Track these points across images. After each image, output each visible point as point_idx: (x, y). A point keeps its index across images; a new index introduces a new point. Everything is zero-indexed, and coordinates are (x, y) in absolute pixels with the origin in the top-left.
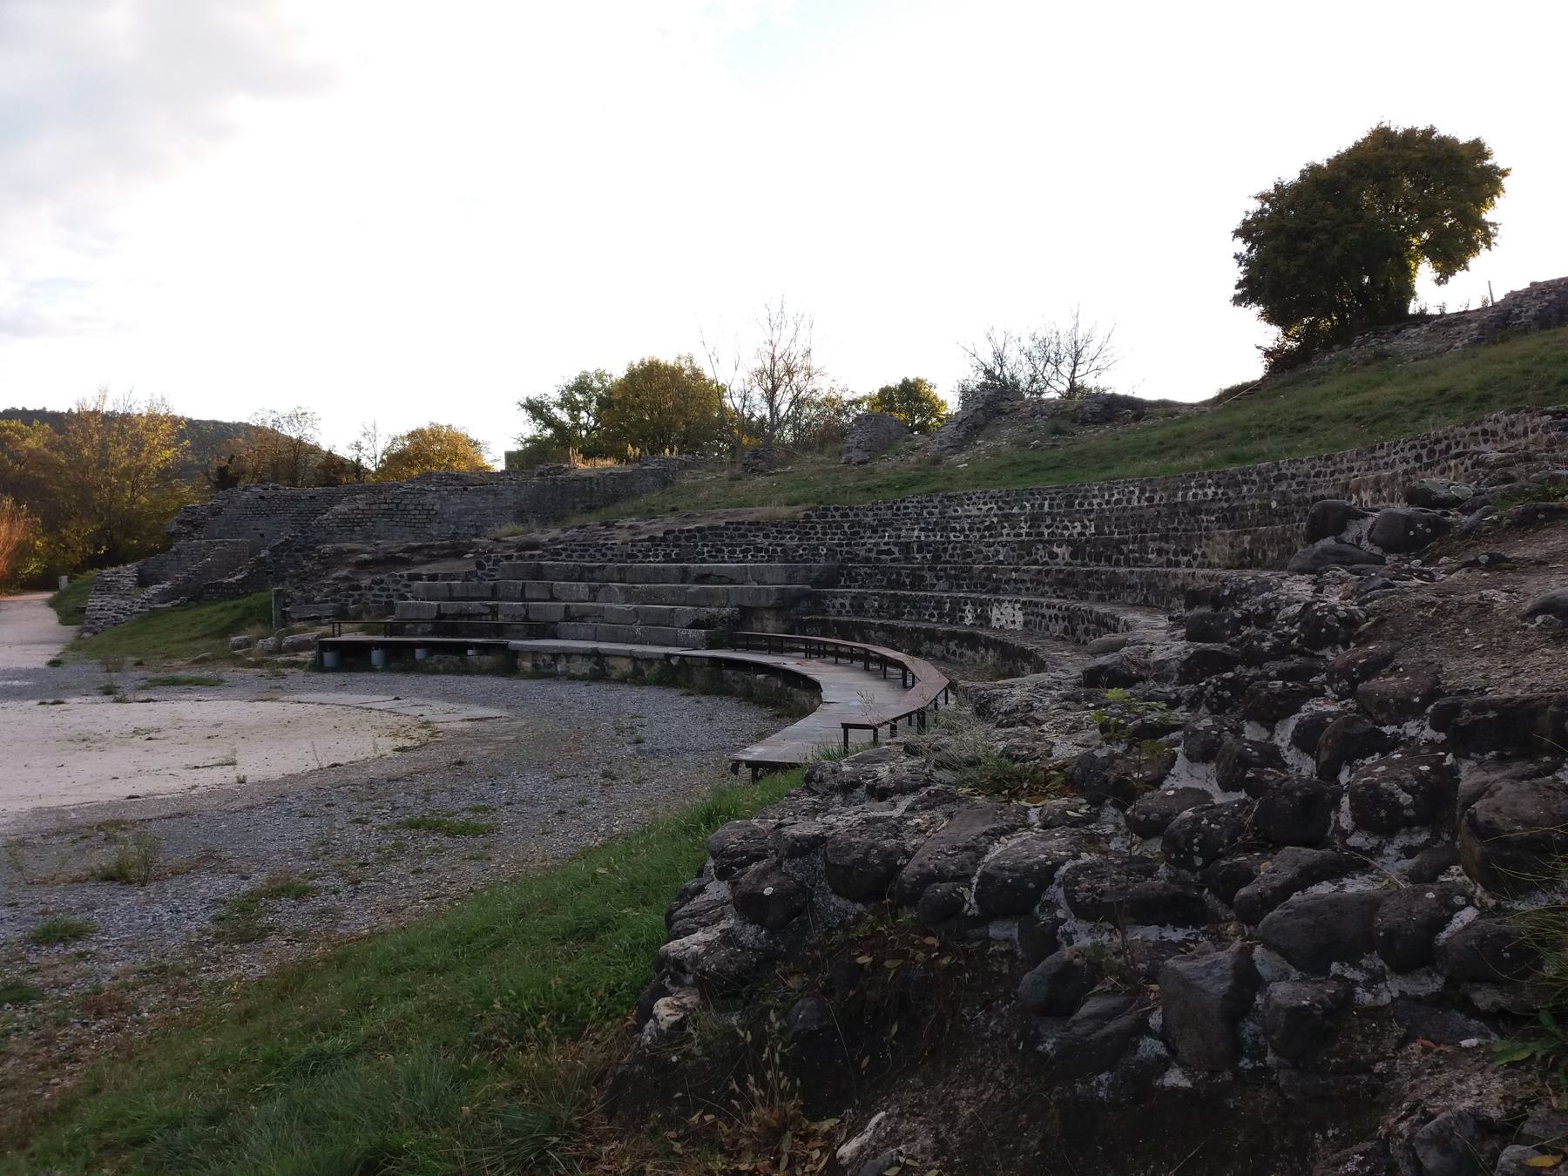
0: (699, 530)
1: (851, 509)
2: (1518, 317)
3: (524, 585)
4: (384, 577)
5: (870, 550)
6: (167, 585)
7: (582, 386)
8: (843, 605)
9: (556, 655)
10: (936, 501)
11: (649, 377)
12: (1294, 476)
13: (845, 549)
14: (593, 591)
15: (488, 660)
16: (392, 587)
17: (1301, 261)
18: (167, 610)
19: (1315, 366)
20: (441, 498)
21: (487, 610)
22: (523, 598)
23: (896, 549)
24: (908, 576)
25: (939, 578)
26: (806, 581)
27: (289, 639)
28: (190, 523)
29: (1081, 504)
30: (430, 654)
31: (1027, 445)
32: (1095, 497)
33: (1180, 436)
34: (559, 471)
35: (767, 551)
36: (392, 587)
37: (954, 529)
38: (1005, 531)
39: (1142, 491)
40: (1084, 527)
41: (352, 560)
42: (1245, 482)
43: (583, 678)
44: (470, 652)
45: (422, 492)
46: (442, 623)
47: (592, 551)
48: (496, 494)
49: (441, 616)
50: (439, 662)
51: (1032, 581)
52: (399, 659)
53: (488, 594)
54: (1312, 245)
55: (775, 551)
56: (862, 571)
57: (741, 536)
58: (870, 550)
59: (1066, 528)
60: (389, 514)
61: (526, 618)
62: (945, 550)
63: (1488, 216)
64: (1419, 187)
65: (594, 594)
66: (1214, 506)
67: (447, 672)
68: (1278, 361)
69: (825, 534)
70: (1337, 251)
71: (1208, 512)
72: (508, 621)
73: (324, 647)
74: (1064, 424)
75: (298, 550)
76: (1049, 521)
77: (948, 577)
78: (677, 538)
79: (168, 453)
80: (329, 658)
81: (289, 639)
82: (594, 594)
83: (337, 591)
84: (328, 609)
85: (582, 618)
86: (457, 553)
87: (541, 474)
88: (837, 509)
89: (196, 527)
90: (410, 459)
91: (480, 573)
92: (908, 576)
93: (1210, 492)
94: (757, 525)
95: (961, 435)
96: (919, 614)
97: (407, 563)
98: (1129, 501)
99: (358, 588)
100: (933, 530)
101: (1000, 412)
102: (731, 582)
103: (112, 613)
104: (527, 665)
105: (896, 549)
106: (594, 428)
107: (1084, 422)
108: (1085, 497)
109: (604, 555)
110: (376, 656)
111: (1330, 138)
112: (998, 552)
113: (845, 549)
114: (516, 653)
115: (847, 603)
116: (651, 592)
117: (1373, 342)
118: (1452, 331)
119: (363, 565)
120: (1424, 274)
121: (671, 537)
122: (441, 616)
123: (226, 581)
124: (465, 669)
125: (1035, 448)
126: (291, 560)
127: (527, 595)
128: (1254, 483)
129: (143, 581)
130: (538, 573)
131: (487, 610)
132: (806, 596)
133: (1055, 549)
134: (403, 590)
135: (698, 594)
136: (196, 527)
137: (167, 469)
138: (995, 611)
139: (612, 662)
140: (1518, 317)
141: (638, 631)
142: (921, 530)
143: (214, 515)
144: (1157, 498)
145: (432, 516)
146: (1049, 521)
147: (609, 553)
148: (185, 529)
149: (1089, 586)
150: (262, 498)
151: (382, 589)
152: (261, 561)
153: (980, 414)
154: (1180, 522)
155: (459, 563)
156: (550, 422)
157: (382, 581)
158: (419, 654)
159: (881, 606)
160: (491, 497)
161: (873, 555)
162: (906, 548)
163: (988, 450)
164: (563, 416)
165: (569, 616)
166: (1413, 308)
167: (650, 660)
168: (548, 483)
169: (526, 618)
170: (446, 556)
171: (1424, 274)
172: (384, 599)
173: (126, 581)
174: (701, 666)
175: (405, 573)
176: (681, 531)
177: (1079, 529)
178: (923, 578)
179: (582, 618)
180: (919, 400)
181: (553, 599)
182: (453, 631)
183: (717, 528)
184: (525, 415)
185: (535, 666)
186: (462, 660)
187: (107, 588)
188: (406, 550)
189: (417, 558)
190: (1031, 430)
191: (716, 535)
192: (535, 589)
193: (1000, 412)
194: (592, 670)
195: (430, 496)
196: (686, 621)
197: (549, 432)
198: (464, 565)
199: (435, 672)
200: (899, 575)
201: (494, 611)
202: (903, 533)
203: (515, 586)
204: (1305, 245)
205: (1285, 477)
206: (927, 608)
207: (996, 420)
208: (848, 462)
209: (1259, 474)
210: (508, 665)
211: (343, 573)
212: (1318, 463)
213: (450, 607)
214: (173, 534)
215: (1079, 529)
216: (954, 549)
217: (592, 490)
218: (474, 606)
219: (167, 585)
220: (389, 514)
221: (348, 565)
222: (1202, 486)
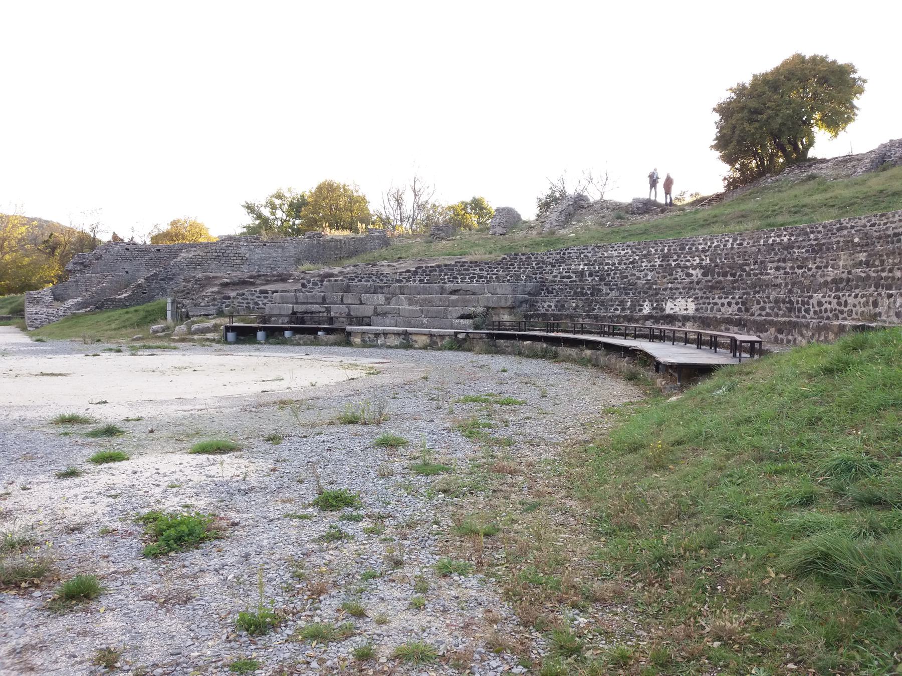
0: (438, 266)
1: (533, 255)
2: (890, 157)
3: (343, 296)
4: (244, 291)
5: (556, 276)
6: (79, 299)
7: (279, 196)
8: (550, 306)
9: (377, 335)
10: (590, 249)
11: (327, 190)
12: (852, 227)
13: (538, 276)
14: (387, 299)
15: (332, 338)
16: (250, 297)
17: (757, 125)
18: (83, 314)
19: (762, 183)
20: (250, 250)
21: (324, 310)
22: (342, 303)
23: (573, 275)
24: (589, 289)
25: (611, 290)
26: (523, 292)
27: (195, 326)
28: (82, 263)
29: (690, 248)
30: (294, 334)
31: (604, 224)
32: (700, 244)
33: (715, 216)
34: (320, 235)
35: (486, 278)
36: (250, 297)
37: (607, 264)
38: (644, 264)
39: (735, 240)
40: (702, 260)
41: (218, 282)
42: (812, 232)
43: (396, 347)
44: (320, 333)
45: (238, 246)
46: (295, 316)
47: (374, 278)
48: (283, 248)
49: (294, 313)
50: (300, 339)
51: (684, 288)
52: (275, 335)
53: (320, 301)
54: (765, 116)
55: (491, 278)
56: (557, 287)
57: (465, 270)
58: (556, 276)
59: (689, 261)
60: (218, 258)
61: (349, 314)
62: (609, 275)
63: (855, 102)
64: (811, 90)
65: (388, 301)
66: (804, 244)
67: (305, 344)
68: (732, 185)
69: (520, 268)
70: (779, 120)
71: (799, 247)
72: (337, 315)
73: (228, 329)
74: (622, 214)
75: (161, 280)
76: (675, 257)
77: (618, 289)
78: (424, 271)
79: (23, 229)
80: (231, 336)
81: (195, 326)
82: (388, 301)
83: (214, 299)
84: (212, 310)
85: (385, 314)
86: (283, 279)
87: (309, 237)
88: (523, 255)
89: (85, 266)
90: (172, 237)
91: (304, 290)
92: (589, 289)
93: (785, 239)
94: (475, 263)
95: (563, 219)
96: (606, 309)
97: (253, 284)
98: (725, 245)
99: (229, 298)
100: (593, 265)
101: (582, 207)
102: (474, 294)
103: (44, 316)
104: (357, 340)
105: (573, 275)
106: (286, 220)
107: (633, 213)
108: (693, 245)
109: (382, 280)
110: (260, 335)
111: (768, 60)
112: (647, 275)
113: (538, 276)
114: (349, 334)
115: (553, 305)
116: (426, 299)
117: (796, 171)
118: (850, 165)
119: (226, 285)
120: (821, 135)
121: (420, 270)
122: (294, 313)
123: (118, 297)
124: (316, 343)
125: (609, 226)
126: (158, 285)
127: (345, 301)
128: (819, 232)
129: (58, 298)
130: (348, 289)
131: (324, 310)
132: (526, 301)
133: (691, 271)
134: (257, 299)
135: (458, 300)
136: (85, 266)
137: (23, 239)
138: (669, 304)
139: (414, 338)
140: (890, 157)
141: (425, 321)
142: (585, 265)
143: (97, 259)
144: (745, 244)
145: (244, 260)
146: (675, 257)
147: (385, 279)
148: (78, 268)
149: (734, 288)
150: (127, 249)
151: (244, 299)
152: (139, 286)
153: (571, 208)
154: (776, 254)
155: (286, 285)
156: (259, 216)
157: (244, 294)
158: (287, 334)
159: (577, 306)
160: (280, 250)
161: (558, 279)
162: (581, 274)
163: (582, 227)
164: (266, 212)
165: (376, 314)
166: (811, 154)
167: (442, 337)
168: (315, 242)
169: (349, 314)
170: (276, 281)
171: (821, 135)
172: (245, 305)
173: (47, 298)
174: (481, 338)
175: (258, 289)
176: (427, 267)
177: (698, 261)
178: (600, 290)
179: (385, 314)
180: (482, 208)
181: (361, 304)
182: (303, 322)
183: (450, 265)
184: (245, 211)
185: (363, 341)
186: (315, 338)
187: (36, 301)
188: (251, 277)
189: (258, 282)
190: (603, 217)
191: (449, 269)
192: (349, 299)
193: (582, 207)
194: (401, 343)
195: (243, 248)
196: (455, 315)
197: (257, 222)
198: (290, 285)
199: (299, 344)
200: (583, 289)
201: (328, 310)
202: (573, 267)
203: (288, 307)
204: (760, 116)
205: (846, 228)
206: (612, 305)
207: (579, 211)
208: (494, 234)
209: (824, 227)
210: (346, 340)
211: (216, 289)
212: (873, 219)
213: (300, 308)
214: (70, 271)
215: (698, 261)
216: (615, 274)
217: (341, 247)
218: (315, 308)
219: (79, 299)
220: (218, 258)
221: (216, 285)
222: (779, 236)
